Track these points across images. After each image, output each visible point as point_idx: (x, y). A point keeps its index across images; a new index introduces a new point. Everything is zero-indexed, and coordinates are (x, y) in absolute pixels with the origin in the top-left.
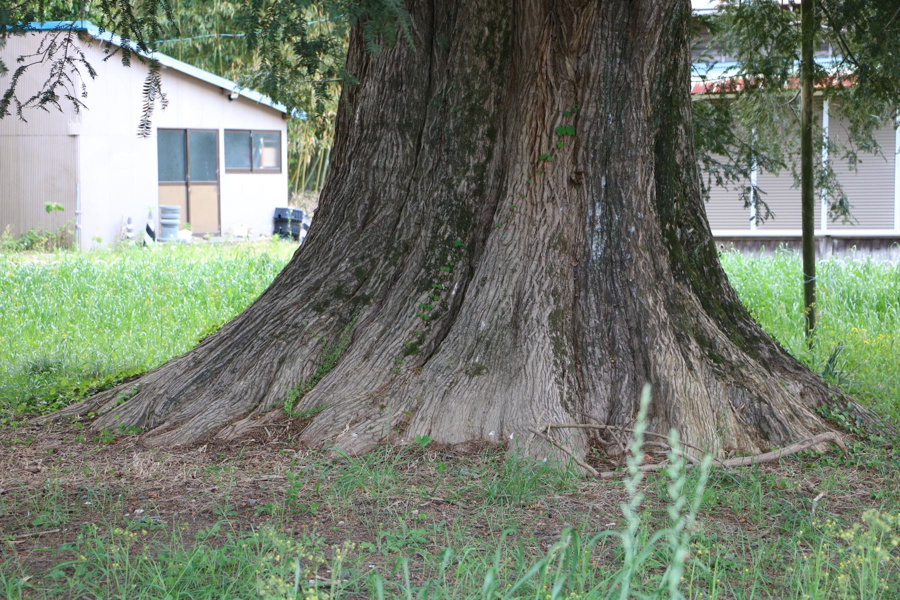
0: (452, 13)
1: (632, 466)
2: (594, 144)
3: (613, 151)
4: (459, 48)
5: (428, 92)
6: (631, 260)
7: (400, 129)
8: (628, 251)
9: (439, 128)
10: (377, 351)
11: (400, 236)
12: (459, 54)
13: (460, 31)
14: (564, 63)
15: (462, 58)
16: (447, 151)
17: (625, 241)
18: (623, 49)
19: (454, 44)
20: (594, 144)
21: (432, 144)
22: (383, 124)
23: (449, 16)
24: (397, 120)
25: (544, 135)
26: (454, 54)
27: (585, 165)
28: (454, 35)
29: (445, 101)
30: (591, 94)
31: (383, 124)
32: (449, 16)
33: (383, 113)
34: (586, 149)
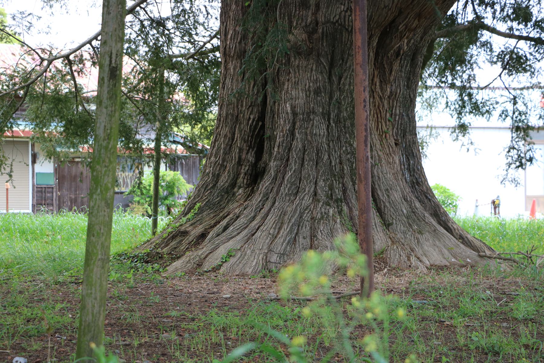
0: (345, 59)
1: (535, 333)
2: (401, 127)
3: (408, 130)
4: (349, 76)
5: (331, 98)
6: (422, 181)
7: (322, 115)
8: (420, 178)
9: (338, 115)
10: (307, 212)
11: (336, 169)
12: (348, 79)
13: (350, 68)
14: (386, 87)
15: (350, 82)
16: (345, 127)
17: (417, 173)
18: (408, 83)
19: (345, 75)
20: (401, 127)
21: (336, 124)
22: (314, 112)
23: (343, 61)
24: (321, 111)
25: (383, 121)
26: (346, 79)
27: (397, 137)
28: (345, 70)
29: (340, 103)
30: (397, 104)
31: (314, 112)
32: (343, 61)
33: (313, 107)
34: (397, 129)
